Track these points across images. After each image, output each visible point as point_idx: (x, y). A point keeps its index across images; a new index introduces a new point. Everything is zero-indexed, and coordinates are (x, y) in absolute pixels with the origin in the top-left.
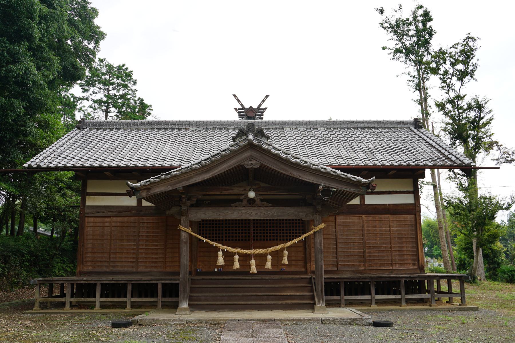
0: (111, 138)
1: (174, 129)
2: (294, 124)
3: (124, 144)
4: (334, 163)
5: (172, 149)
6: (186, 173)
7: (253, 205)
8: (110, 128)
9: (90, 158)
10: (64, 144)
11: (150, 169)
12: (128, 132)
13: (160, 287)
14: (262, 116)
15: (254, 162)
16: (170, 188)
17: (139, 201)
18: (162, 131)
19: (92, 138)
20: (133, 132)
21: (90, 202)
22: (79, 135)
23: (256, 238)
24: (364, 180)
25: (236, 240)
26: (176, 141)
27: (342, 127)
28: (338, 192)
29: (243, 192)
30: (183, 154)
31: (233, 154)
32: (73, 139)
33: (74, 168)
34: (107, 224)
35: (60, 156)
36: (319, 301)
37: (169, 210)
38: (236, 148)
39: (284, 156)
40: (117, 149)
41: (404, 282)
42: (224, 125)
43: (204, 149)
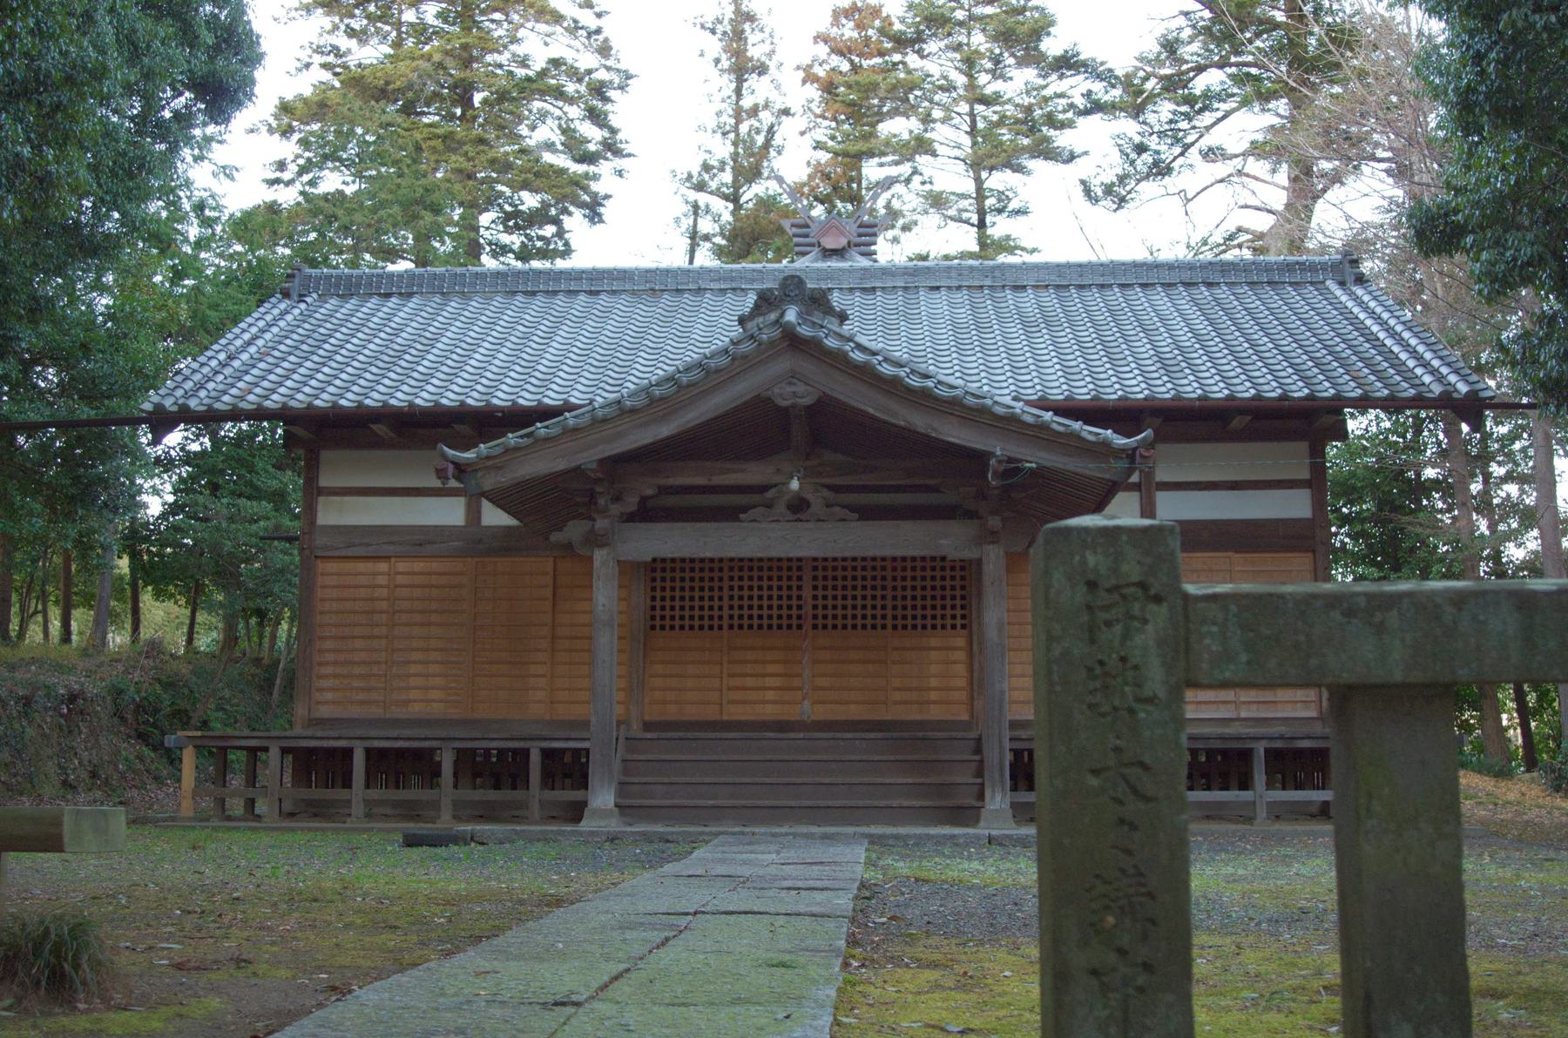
0: (385, 325)
1: (577, 292)
2: (954, 274)
3: (425, 341)
4: (1057, 394)
5: (615, 360)
6: (605, 420)
7: (802, 517)
8: (380, 295)
9: (329, 383)
10: (249, 343)
11: (503, 412)
12: (435, 306)
13: (535, 758)
14: (873, 248)
15: (800, 388)
16: (562, 465)
17: (474, 514)
18: (539, 301)
19: (329, 326)
20: (453, 304)
21: (332, 514)
22: (289, 317)
23: (820, 622)
24: (1120, 441)
25: (760, 627)
26: (583, 332)
27: (1100, 281)
28: (1040, 473)
29: (777, 479)
30: (601, 370)
31: (735, 363)
32: (275, 330)
33: (284, 415)
34: (382, 580)
35: (240, 379)
36: (993, 791)
37: (560, 529)
38: (746, 347)
39: (887, 370)
40: (407, 357)
41: (1262, 751)
42: (732, 279)
43: (665, 353)
